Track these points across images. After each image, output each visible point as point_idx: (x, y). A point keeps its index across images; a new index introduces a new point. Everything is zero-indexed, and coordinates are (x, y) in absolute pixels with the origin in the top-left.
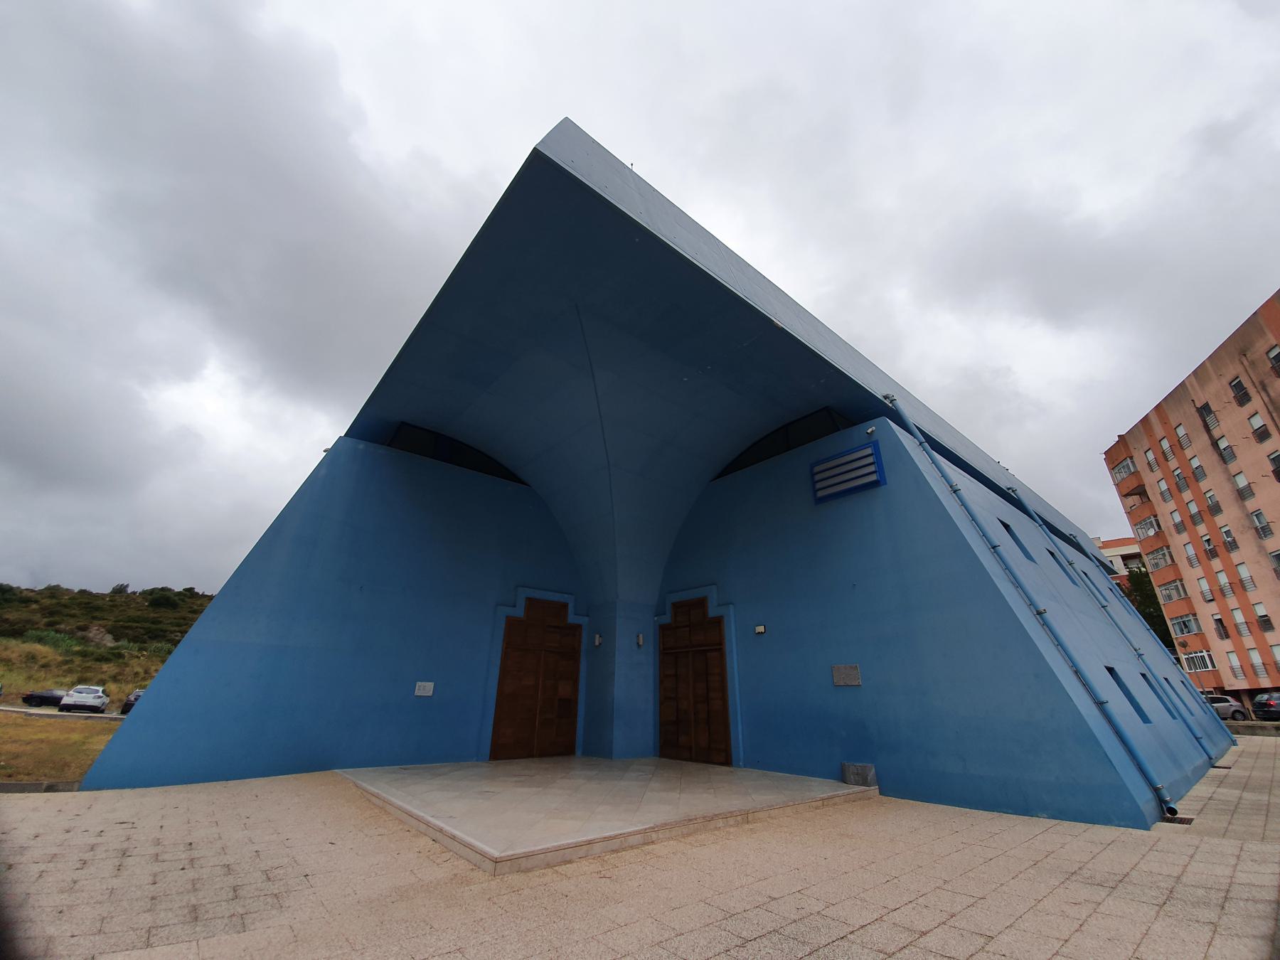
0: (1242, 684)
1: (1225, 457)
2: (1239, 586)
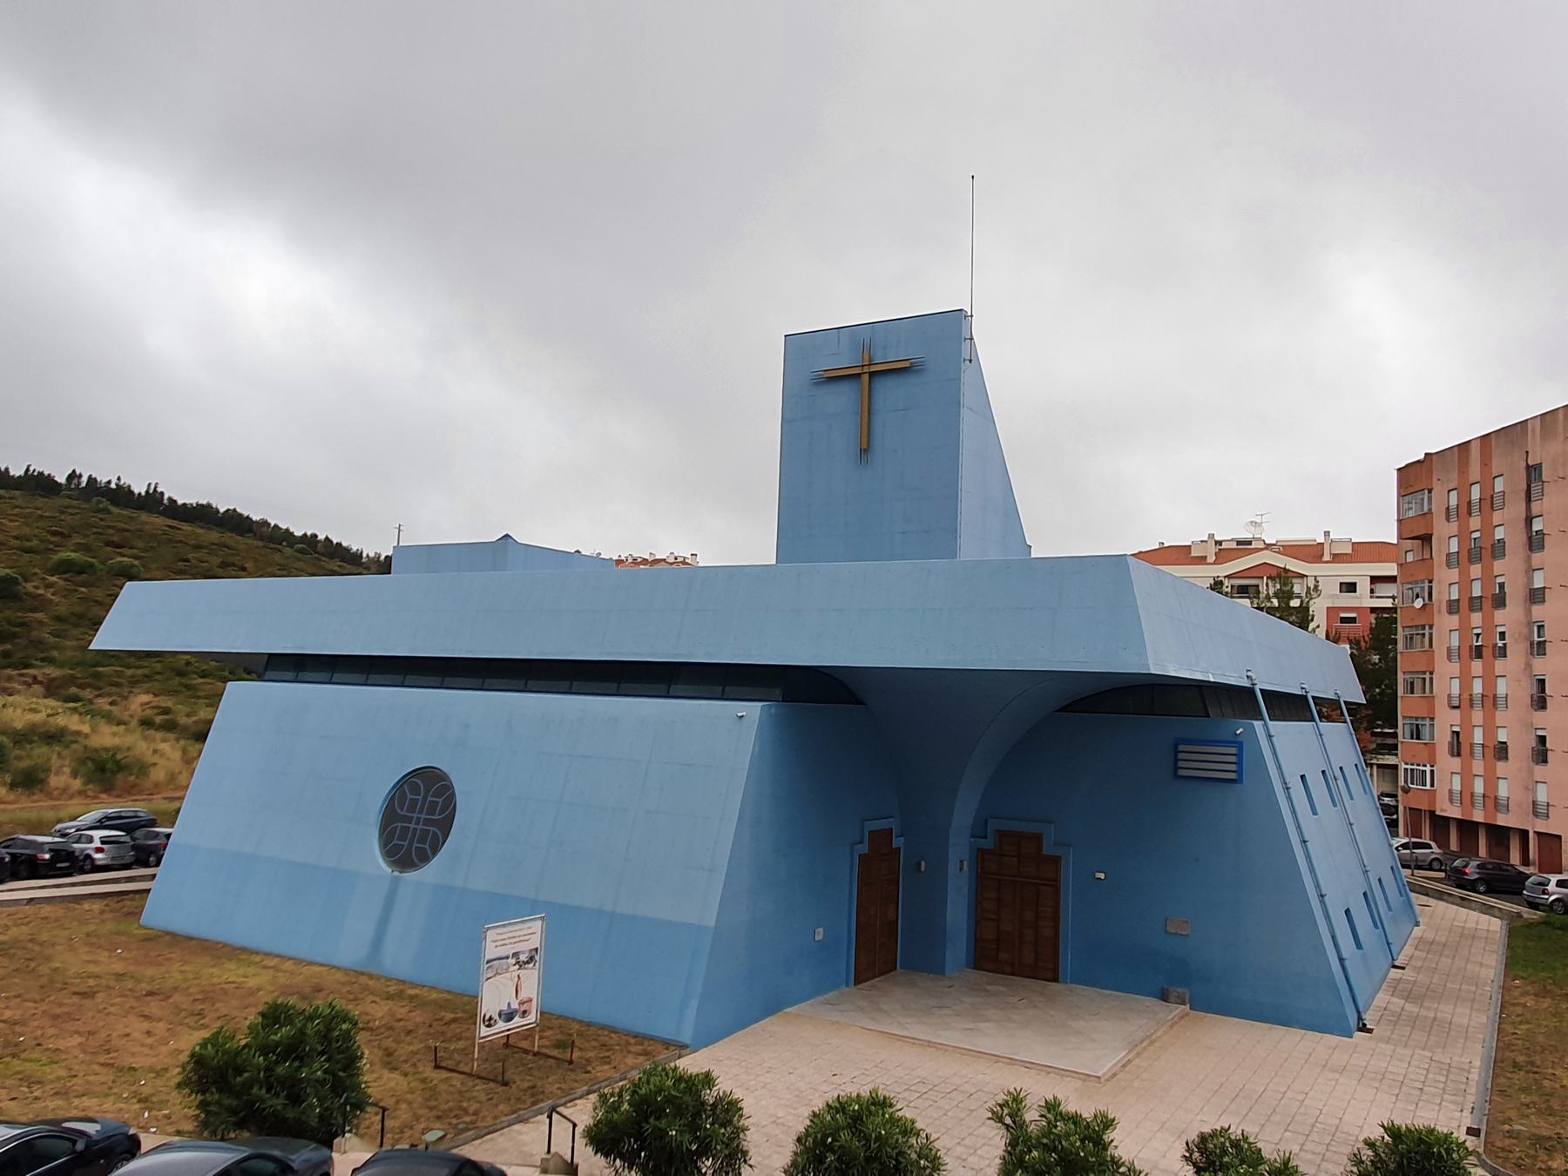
0: (1454, 812)
1: (1535, 542)
2: (1491, 701)
